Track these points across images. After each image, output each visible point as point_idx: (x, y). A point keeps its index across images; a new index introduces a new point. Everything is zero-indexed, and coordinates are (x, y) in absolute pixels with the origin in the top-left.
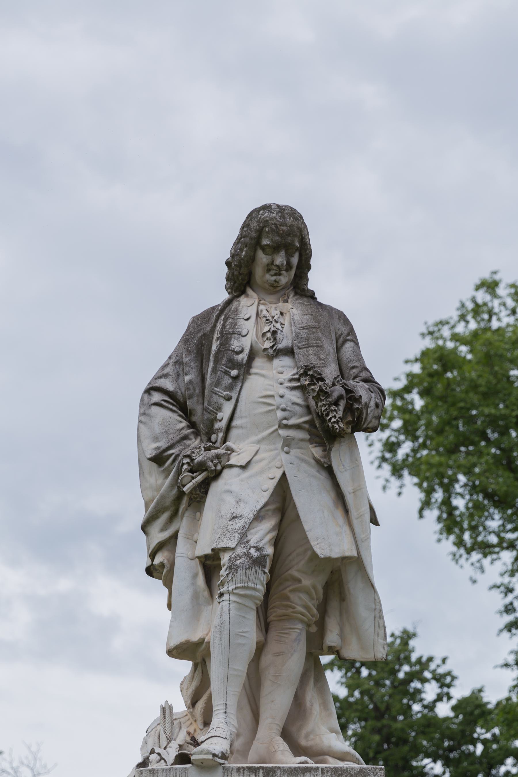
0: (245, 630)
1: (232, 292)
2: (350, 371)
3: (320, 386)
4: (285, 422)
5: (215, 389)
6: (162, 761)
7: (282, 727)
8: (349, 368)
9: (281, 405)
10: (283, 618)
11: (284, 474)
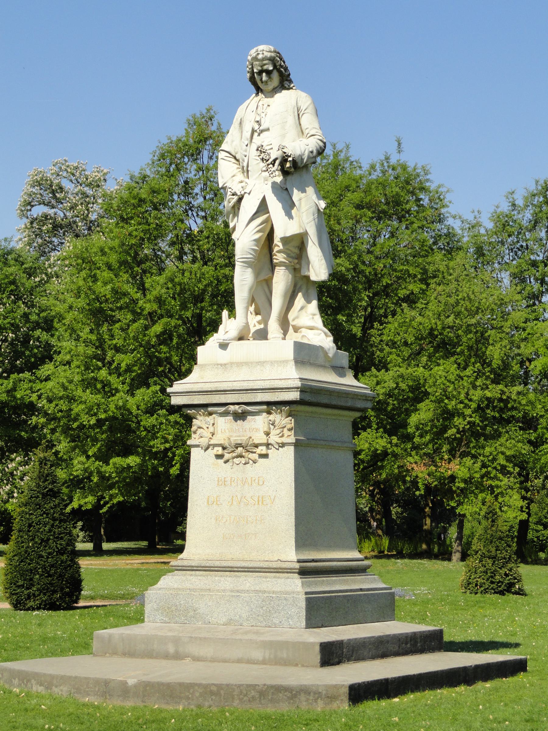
11: (264, 197)
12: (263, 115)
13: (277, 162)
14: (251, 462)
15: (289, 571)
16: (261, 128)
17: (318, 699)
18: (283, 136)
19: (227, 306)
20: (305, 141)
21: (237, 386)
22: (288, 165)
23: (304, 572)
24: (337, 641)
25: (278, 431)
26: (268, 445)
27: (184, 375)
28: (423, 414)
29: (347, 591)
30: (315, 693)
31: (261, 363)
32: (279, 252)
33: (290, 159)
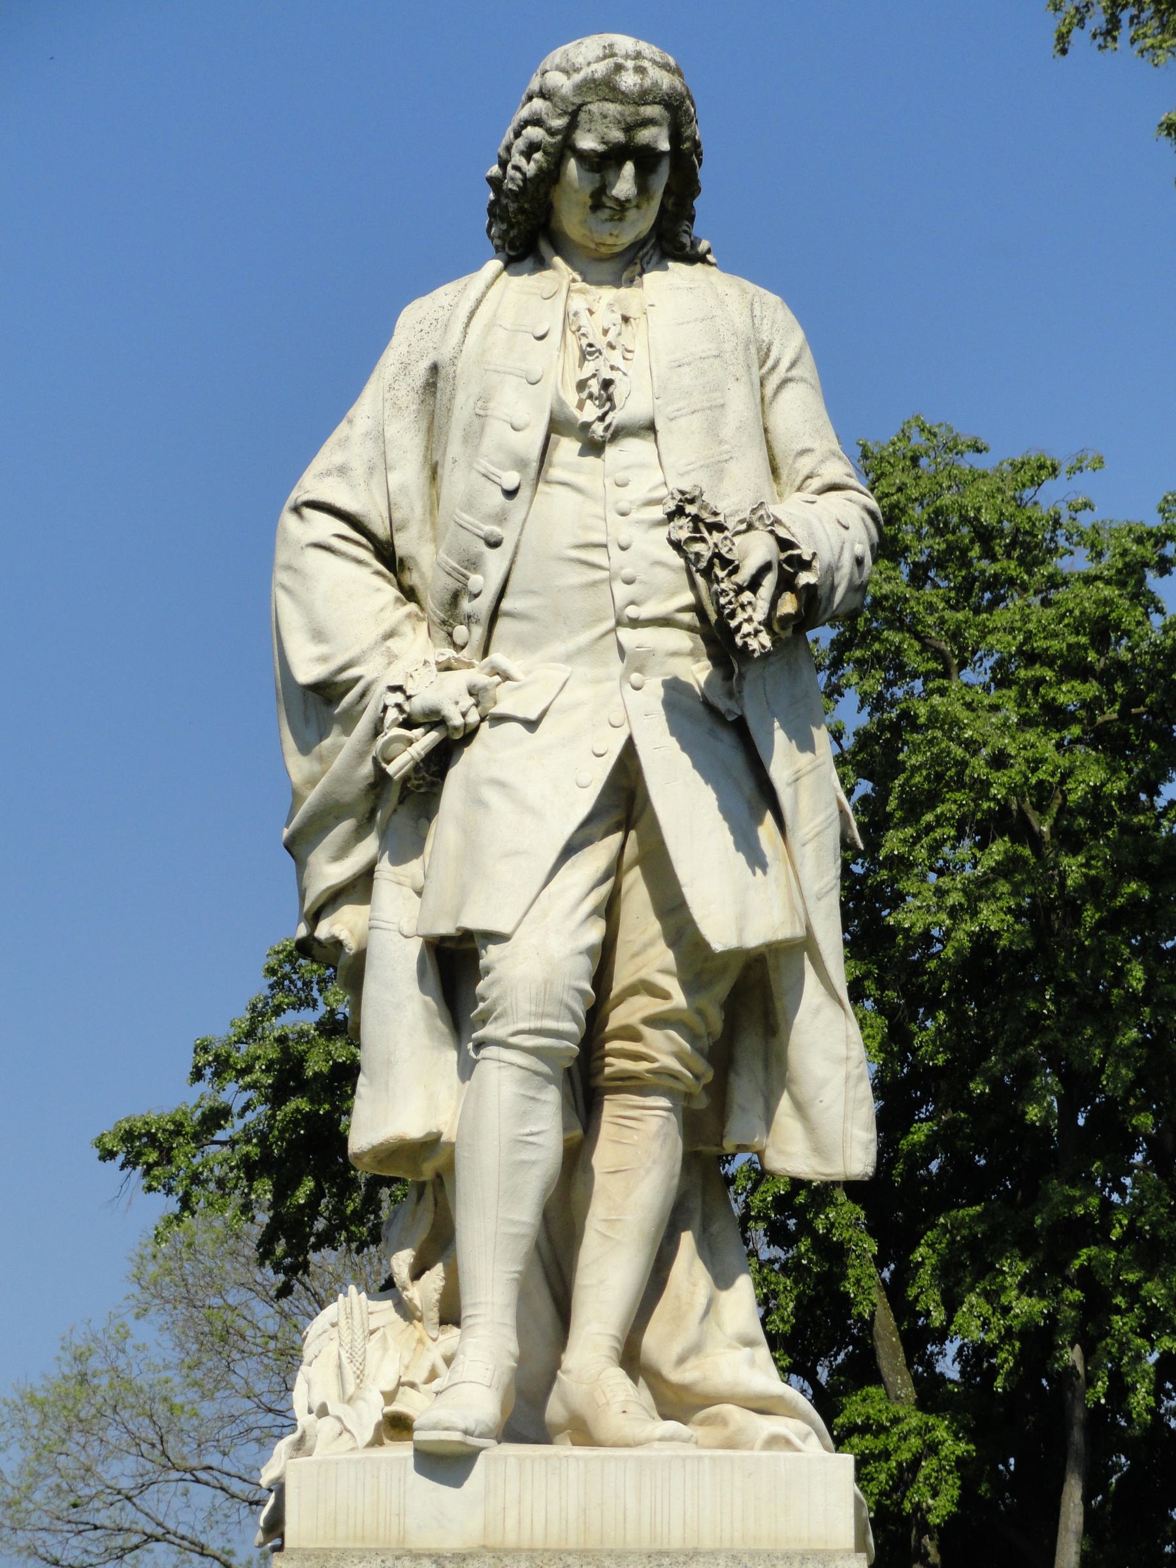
0: (535, 1129)
1: (503, 248)
2: (794, 462)
3: (716, 545)
4: (632, 611)
5: (464, 515)
6: (346, 1436)
7: (623, 1341)
8: (794, 453)
9: (622, 568)
10: (628, 1083)
11: (629, 750)
16: (615, 418)
19: (354, 1278)
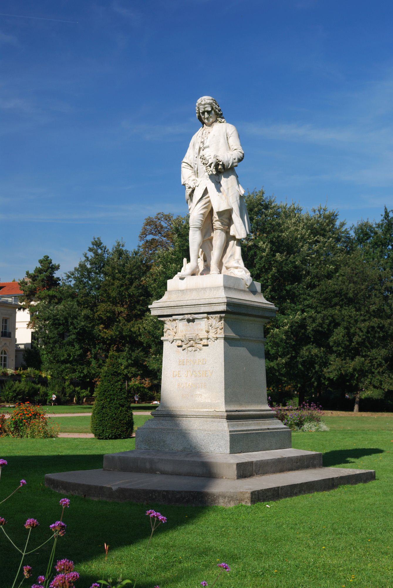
11: (206, 189)
12: (206, 138)
13: (213, 165)
14: (198, 350)
15: (221, 417)
17: (230, 501)
18: (218, 150)
20: (231, 152)
21: (189, 303)
22: (220, 167)
23: (230, 418)
24: (248, 462)
25: (214, 330)
26: (208, 339)
27: (160, 296)
28: (338, 334)
29: (258, 430)
30: (228, 497)
31: (204, 289)
32: (216, 221)
33: (221, 163)
